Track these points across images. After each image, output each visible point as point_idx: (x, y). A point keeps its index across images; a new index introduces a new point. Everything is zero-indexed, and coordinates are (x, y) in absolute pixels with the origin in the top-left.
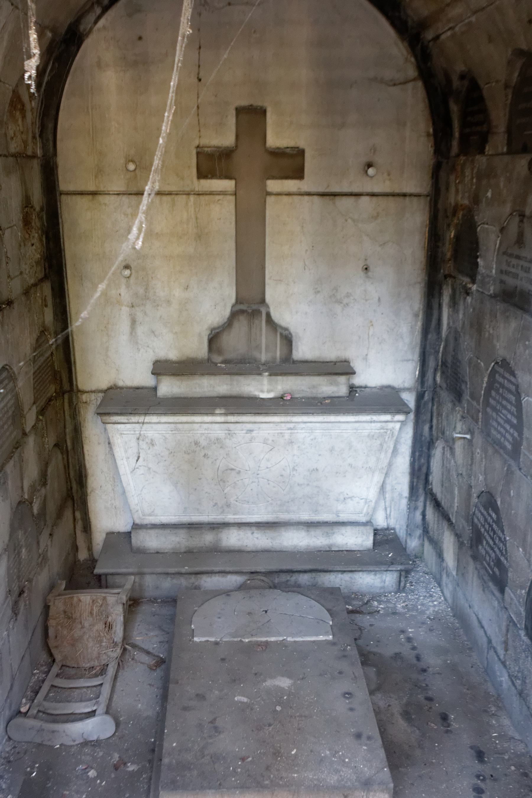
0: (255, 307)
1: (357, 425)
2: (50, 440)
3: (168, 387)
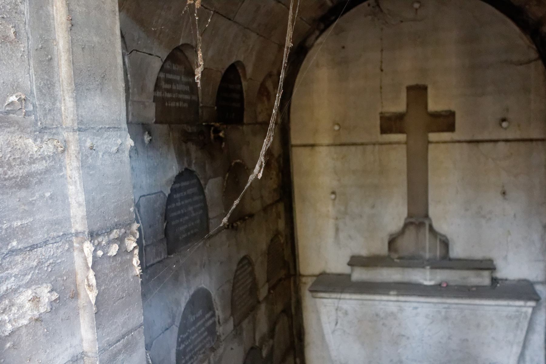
0: (421, 220)
1: (497, 308)
2: (279, 307)
3: (359, 275)
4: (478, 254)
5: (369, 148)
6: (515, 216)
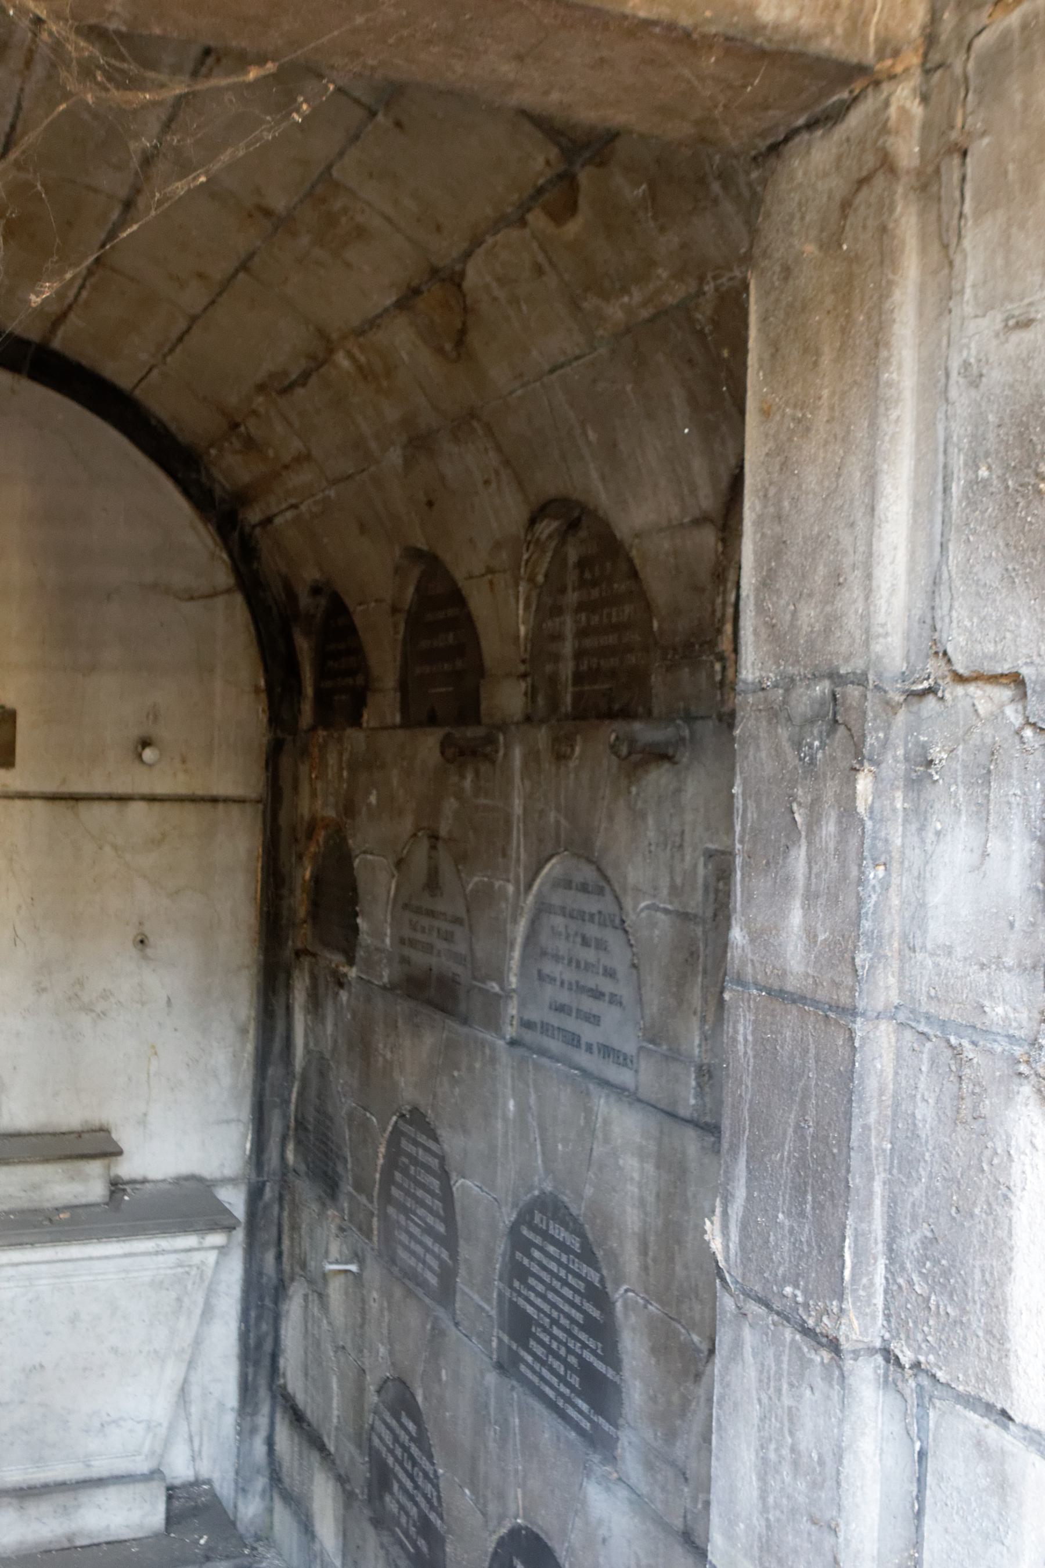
1: (127, 1261)
4: (69, 1115)
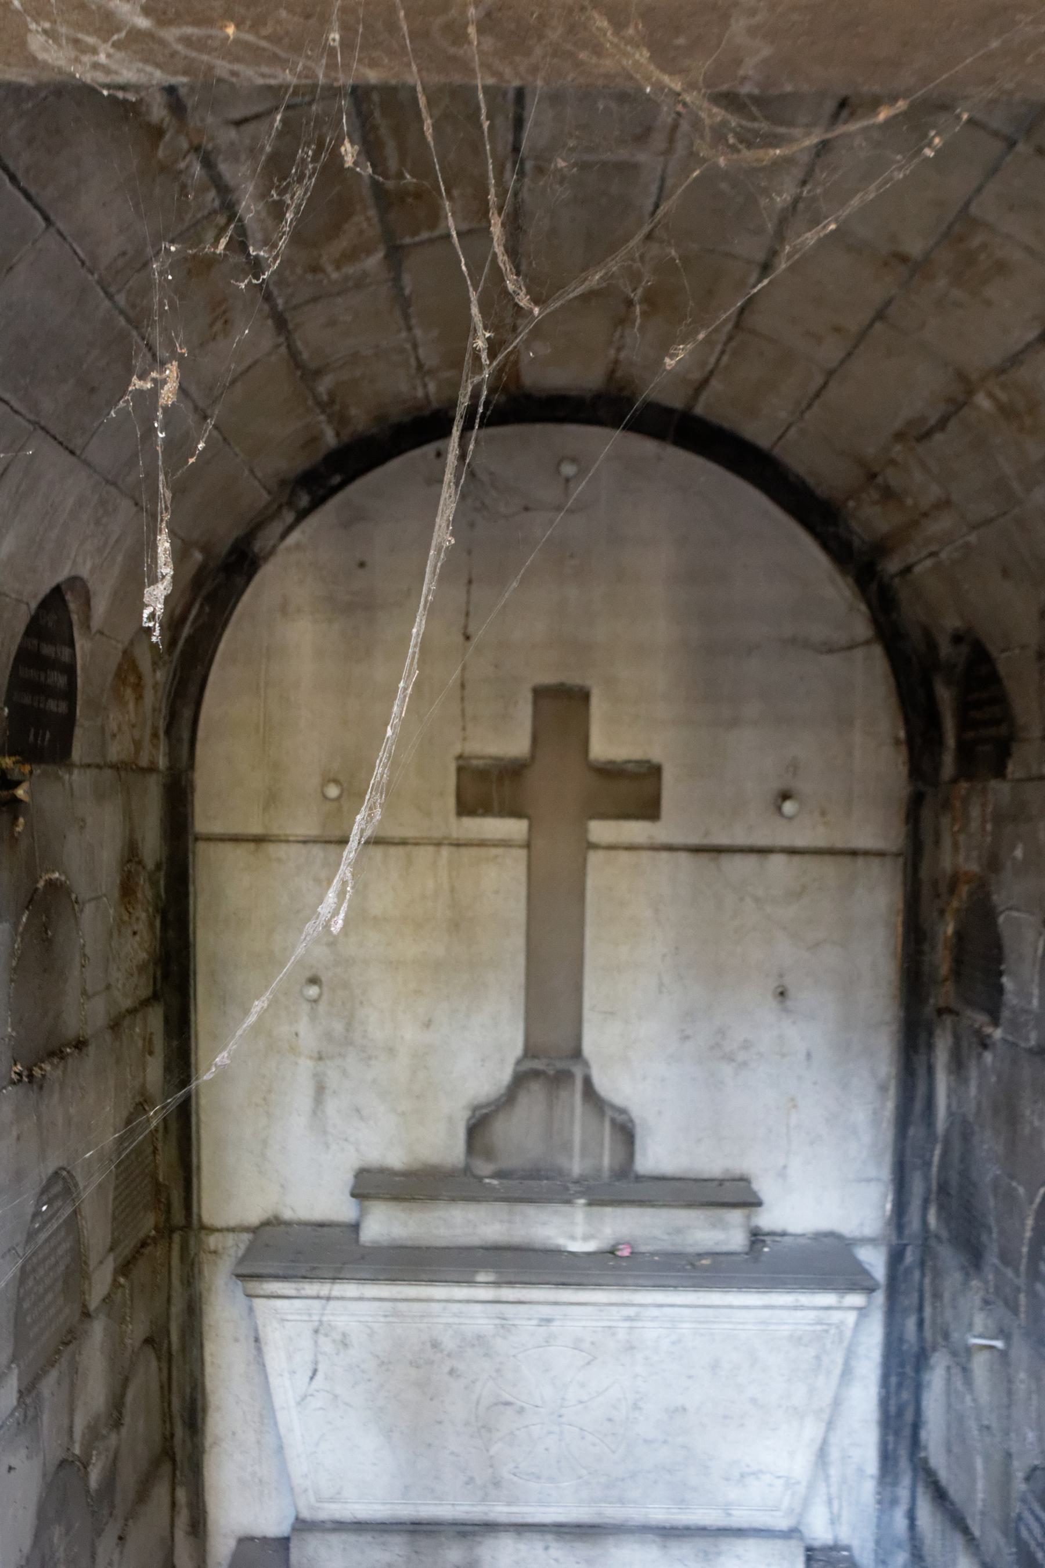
0: (560, 1065)
1: (767, 1313)
2: (137, 1330)
3: (384, 1224)
5: (424, 854)
6: (809, 1055)
